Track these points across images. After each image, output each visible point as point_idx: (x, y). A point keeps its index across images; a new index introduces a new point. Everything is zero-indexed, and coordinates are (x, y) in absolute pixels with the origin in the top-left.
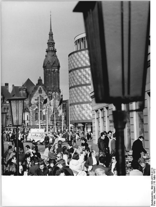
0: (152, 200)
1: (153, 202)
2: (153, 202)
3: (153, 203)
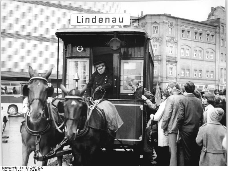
0: (8, 168)
1: (5, 169)
2: (5, 169)
3: (4, 169)
